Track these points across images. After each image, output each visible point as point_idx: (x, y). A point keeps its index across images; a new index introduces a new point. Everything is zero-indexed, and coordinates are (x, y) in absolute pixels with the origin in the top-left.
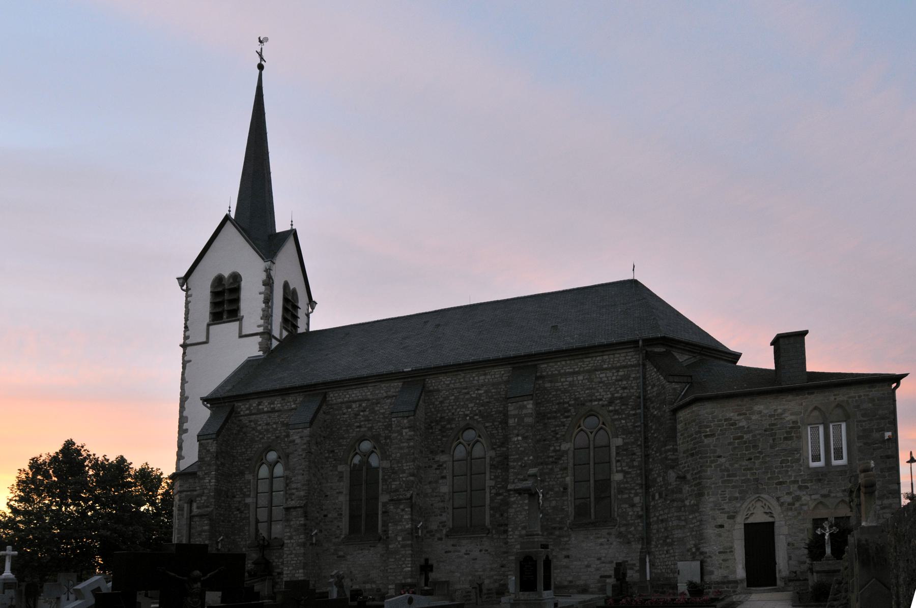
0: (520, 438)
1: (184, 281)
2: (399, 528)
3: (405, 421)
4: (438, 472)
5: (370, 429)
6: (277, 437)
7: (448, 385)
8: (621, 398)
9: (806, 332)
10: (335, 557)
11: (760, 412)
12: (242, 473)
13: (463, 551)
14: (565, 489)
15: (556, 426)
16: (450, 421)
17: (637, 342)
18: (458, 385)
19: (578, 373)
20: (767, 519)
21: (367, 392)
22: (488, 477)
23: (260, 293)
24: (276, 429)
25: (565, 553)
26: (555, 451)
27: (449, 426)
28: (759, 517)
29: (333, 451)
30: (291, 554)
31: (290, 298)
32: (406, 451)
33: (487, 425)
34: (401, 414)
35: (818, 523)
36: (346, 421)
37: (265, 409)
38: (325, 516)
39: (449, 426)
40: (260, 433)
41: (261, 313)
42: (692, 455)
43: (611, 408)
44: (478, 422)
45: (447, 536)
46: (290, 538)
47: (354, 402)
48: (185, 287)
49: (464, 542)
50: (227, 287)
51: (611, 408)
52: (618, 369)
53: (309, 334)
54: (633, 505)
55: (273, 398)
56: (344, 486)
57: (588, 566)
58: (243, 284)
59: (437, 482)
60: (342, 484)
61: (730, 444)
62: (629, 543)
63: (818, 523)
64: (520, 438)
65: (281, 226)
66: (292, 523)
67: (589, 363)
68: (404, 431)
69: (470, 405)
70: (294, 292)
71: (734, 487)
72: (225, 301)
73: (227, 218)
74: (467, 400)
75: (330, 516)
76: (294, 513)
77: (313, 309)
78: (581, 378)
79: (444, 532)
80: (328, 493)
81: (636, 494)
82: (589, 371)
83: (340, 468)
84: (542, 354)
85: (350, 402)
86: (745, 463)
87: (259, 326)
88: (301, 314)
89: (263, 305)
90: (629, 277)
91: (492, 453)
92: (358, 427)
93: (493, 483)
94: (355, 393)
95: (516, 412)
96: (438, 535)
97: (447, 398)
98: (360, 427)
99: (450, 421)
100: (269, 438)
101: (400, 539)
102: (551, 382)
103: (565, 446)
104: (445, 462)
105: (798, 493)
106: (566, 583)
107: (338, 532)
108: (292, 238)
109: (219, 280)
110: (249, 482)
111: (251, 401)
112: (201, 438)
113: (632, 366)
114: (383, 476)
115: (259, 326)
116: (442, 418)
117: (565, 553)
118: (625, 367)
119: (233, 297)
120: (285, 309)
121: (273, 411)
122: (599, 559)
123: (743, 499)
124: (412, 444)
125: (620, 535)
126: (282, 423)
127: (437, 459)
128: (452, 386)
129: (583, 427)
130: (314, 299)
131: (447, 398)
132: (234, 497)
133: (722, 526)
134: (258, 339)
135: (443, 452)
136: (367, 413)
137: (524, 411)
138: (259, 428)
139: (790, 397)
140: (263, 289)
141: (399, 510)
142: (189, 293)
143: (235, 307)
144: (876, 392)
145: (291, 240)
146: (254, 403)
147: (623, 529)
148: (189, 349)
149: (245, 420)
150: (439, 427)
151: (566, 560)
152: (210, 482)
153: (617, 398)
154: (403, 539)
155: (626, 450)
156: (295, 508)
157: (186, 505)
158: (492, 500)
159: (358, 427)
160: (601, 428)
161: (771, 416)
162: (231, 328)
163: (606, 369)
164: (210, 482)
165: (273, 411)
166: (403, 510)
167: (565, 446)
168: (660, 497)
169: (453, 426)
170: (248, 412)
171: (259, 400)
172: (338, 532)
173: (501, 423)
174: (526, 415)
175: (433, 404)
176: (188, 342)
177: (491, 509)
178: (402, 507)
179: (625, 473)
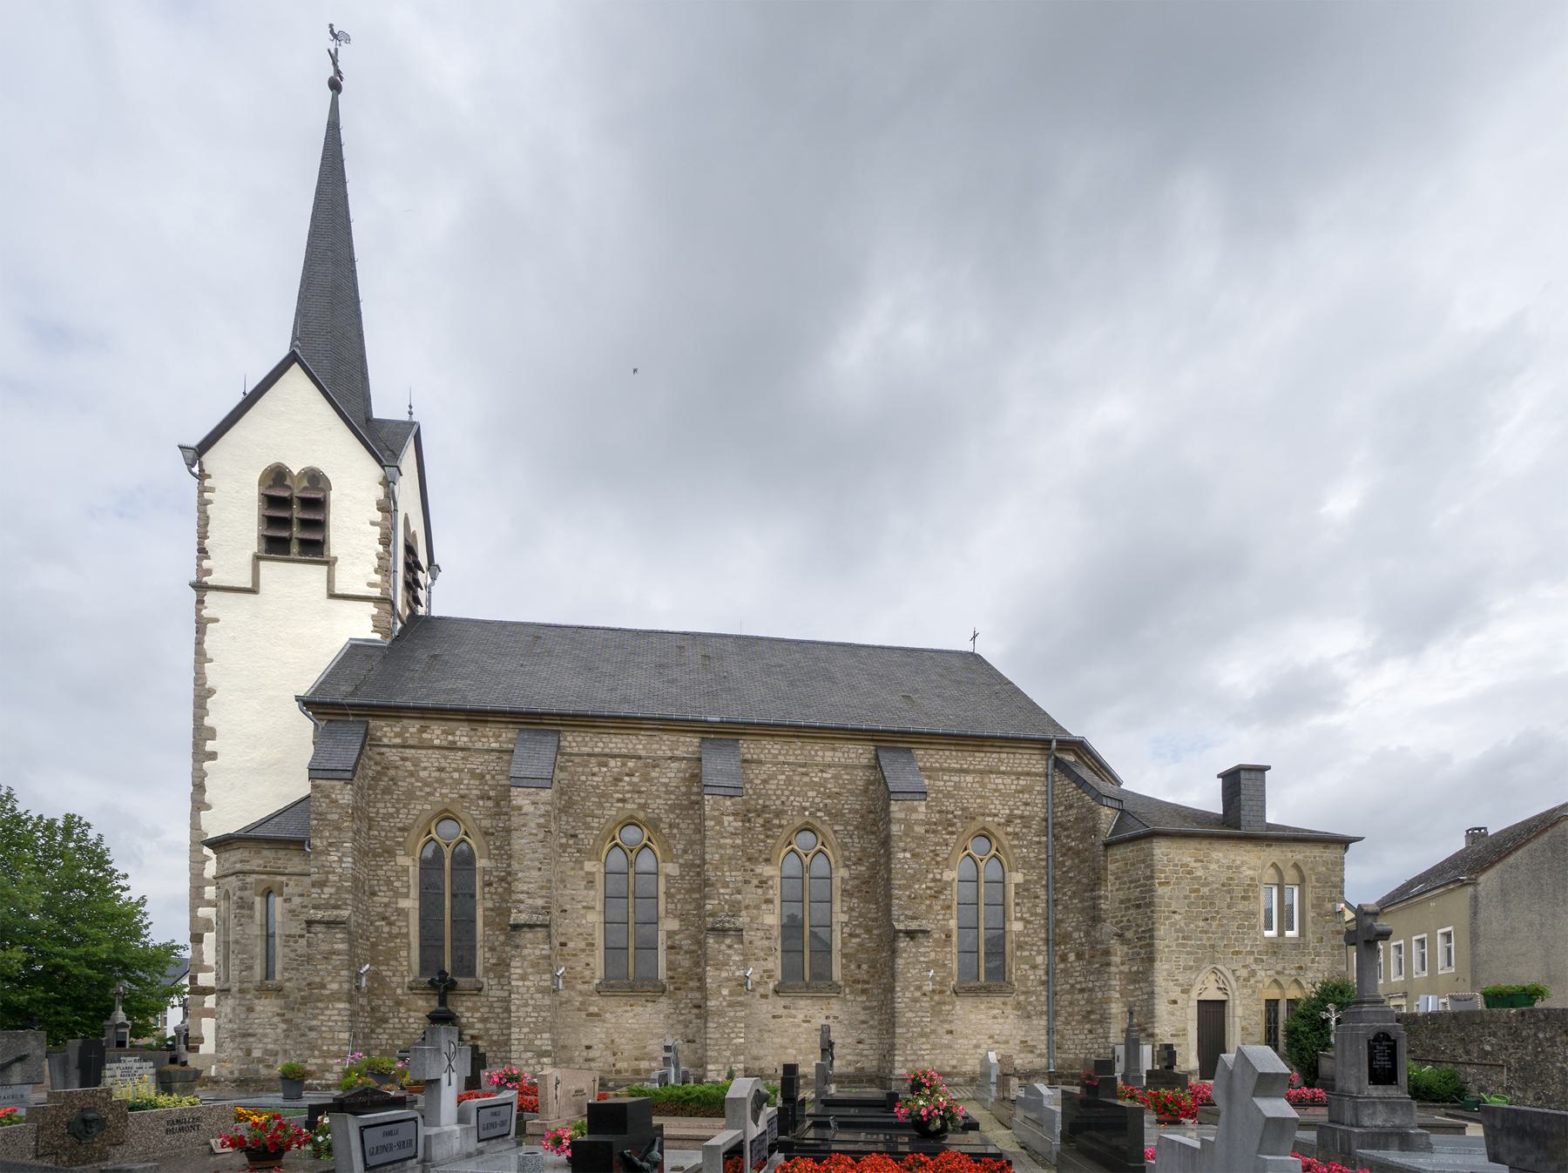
0: (908, 855)
2: (724, 974)
3: (728, 803)
4: (760, 891)
5: (643, 807)
6: (462, 797)
7: (776, 756)
8: (1022, 817)
9: (1269, 768)
10: (583, 1015)
11: (1218, 862)
12: (390, 853)
13: (801, 1017)
14: (948, 936)
15: (936, 844)
16: (779, 814)
17: (1050, 742)
18: (791, 759)
19: (966, 771)
20: (1220, 996)
21: (638, 744)
22: (837, 906)
23: (373, 524)
24: (459, 782)
25: (947, 1027)
26: (934, 880)
27: (776, 822)
28: (1213, 994)
29: (574, 836)
30: (526, 1005)
32: (730, 851)
33: (837, 828)
34: (722, 791)
35: (1272, 1005)
36: (598, 787)
37: (437, 742)
38: (563, 944)
39: (776, 822)
40: (426, 784)
41: (376, 561)
42: (1138, 906)
43: (1009, 829)
44: (823, 822)
45: (776, 992)
46: (523, 978)
47: (614, 756)
48: (196, 469)
49: (802, 1003)
50: (297, 493)
51: (1009, 829)
52: (1019, 775)
53: (429, 620)
54: (1034, 967)
55: (453, 725)
56: (596, 896)
57: (977, 1046)
58: (333, 496)
59: (757, 907)
60: (592, 893)
61: (1186, 897)
62: (1029, 1017)
63: (1272, 1005)
64: (908, 855)
66: (526, 952)
67: (981, 760)
68: (726, 819)
69: (811, 794)
71: (1188, 953)
72: (294, 520)
74: (806, 784)
75: (571, 945)
76: (529, 935)
77: (434, 579)
78: (969, 779)
79: (771, 986)
80: (568, 907)
81: (1039, 953)
82: (981, 772)
83: (589, 866)
84: (922, 734)
85: (606, 755)
86: (1201, 924)
87: (371, 585)
89: (381, 548)
90: (967, 647)
91: (843, 873)
92: (619, 800)
93: (845, 918)
94: (617, 743)
95: (902, 815)
96: (761, 990)
97: (772, 777)
98: (623, 800)
99: (779, 814)
100: (445, 795)
101: (725, 992)
102: (929, 778)
103: (949, 875)
104: (772, 877)
105: (1254, 966)
106: (948, 1069)
107: (587, 973)
109: (277, 475)
110: (406, 870)
111: (405, 722)
112: (314, 774)
113: (1036, 775)
114: (668, 888)
115: (371, 585)
116: (764, 806)
117: (947, 1027)
118: (1028, 774)
121: (452, 747)
122: (991, 1037)
123: (1198, 969)
124: (739, 842)
125: (1018, 1006)
126: (472, 773)
127: (758, 871)
128: (781, 758)
129: (434, 835)
131: (772, 777)
132: (374, 894)
133: (1175, 1002)
134: (371, 609)
135: (767, 860)
136: (635, 779)
137: (914, 816)
138: (423, 774)
139: (1249, 847)
140: (378, 516)
141: (723, 947)
142: (207, 483)
144: (1330, 854)
146: (413, 727)
147: (1022, 998)
148: (210, 597)
149: (393, 755)
150: (761, 821)
151: (949, 1037)
152: (340, 861)
153: (1017, 817)
154: (731, 994)
155: (1027, 890)
156: (531, 926)
157: (258, 900)
158: (844, 944)
159: (619, 800)
160: (820, 851)
161: (1229, 868)
162: (310, 576)
163: (1003, 773)
164: (340, 861)
165: (452, 747)
166: (730, 947)
167: (949, 875)
168: (1079, 956)
169: (784, 822)
170: (398, 741)
171: (422, 723)
172: (587, 973)
173: (857, 828)
174: (917, 822)
175: (751, 782)
176: (208, 580)
177: (844, 956)
178: (728, 941)
179: (1027, 922)
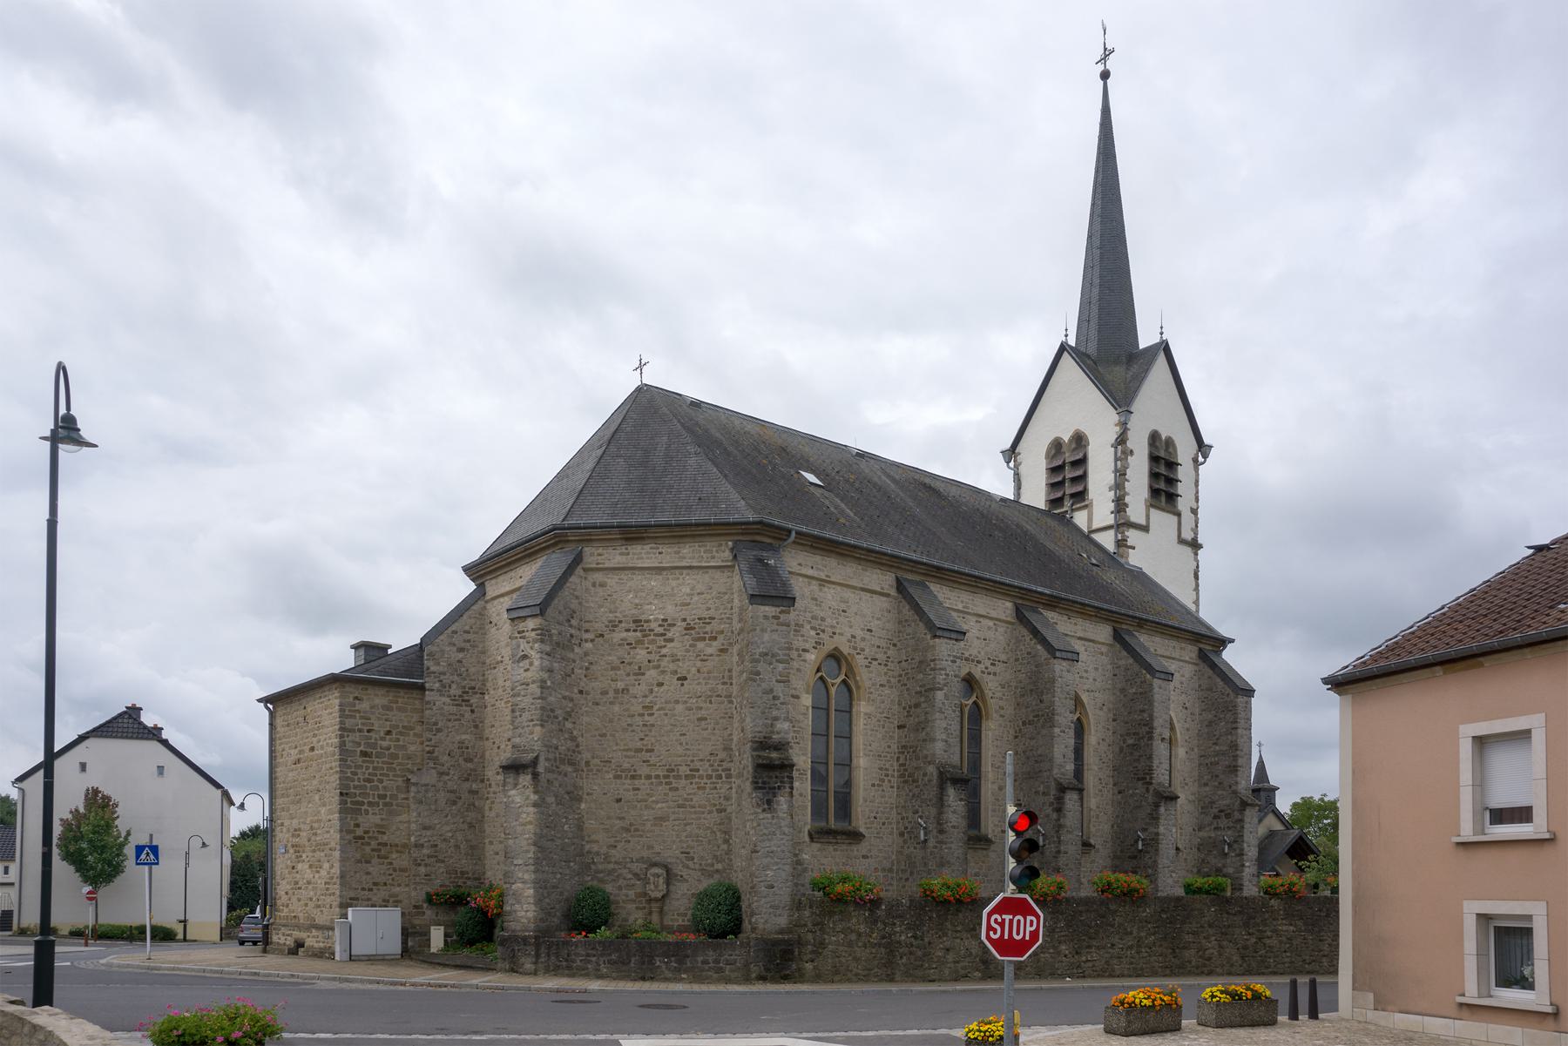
1: (1011, 453)
9: (1232, 641)
31: (1162, 454)
65: (1146, 339)
70: (1169, 443)
73: (1063, 348)
77: (1205, 457)
88: (1184, 472)
108: (1162, 358)
109: (1057, 446)
112: (515, 614)
119: (1079, 473)
120: (1154, 476)
130: (1207, 441)
143: (1080, 488)
145: (1161, 359)
